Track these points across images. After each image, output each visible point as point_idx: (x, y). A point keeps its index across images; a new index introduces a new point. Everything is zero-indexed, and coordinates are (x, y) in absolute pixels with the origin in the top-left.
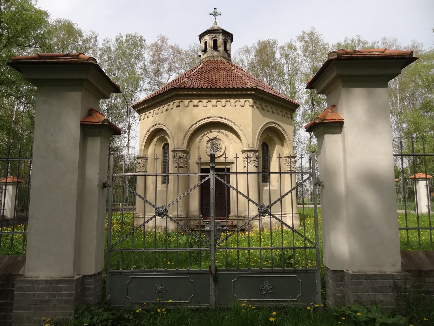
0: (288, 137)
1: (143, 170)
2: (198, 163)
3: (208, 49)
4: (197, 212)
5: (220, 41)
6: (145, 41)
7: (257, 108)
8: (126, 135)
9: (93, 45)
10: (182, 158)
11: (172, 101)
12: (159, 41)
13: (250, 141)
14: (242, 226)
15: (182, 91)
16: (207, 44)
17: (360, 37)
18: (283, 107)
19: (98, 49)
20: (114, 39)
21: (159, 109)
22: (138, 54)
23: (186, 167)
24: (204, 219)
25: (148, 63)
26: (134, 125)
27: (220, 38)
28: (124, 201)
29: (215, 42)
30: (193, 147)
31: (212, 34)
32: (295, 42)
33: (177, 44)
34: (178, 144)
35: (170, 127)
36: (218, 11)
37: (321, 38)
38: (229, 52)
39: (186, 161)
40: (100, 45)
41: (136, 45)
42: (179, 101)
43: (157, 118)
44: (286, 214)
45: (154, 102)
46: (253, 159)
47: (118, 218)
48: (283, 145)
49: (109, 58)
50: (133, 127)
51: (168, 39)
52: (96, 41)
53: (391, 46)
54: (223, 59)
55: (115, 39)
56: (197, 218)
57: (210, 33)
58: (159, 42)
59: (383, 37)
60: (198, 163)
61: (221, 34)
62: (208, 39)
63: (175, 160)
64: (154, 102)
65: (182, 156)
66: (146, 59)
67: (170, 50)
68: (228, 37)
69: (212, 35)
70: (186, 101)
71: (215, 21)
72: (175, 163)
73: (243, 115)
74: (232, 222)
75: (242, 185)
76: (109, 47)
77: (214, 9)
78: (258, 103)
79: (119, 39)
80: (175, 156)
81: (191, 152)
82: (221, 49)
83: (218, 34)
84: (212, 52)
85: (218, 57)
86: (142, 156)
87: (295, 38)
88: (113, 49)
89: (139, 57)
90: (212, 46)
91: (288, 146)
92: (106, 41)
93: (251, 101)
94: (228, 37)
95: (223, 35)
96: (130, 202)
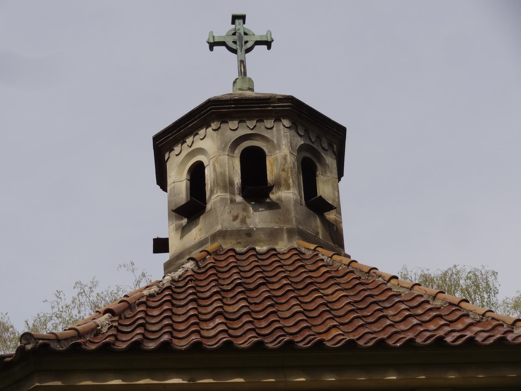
3: (215, 198)
5: (281, 149)
16: (209, 173)
29: (253, 163)
31: (233, 124)
54: (307, 247)
57: (224, 118)
62: (212, 148)
68: (322, 139)
69: (233, 130)
71: (243, 73)
77: (235, 18)
82: (289, 195)
83: (269, 123)
85: (273, 235)
90: (237, 180)
94: (322, 139)
95: (294, 126)
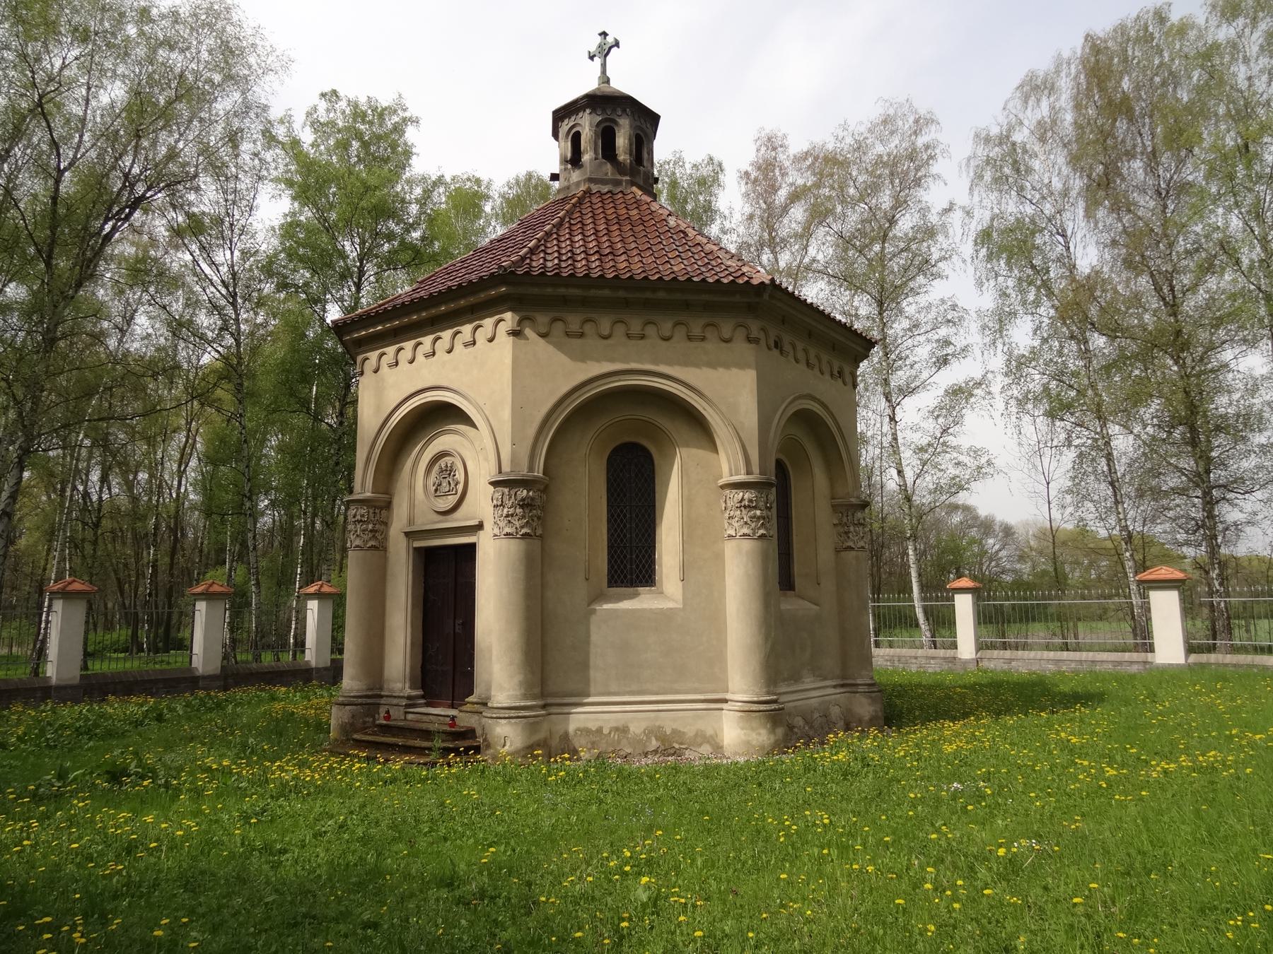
44: (726, 701)
51: (785, 136)
53: (1075, 53)
60: (407, 534)
65: (358, 517)
93: (509, 318)
94: (647, 120)
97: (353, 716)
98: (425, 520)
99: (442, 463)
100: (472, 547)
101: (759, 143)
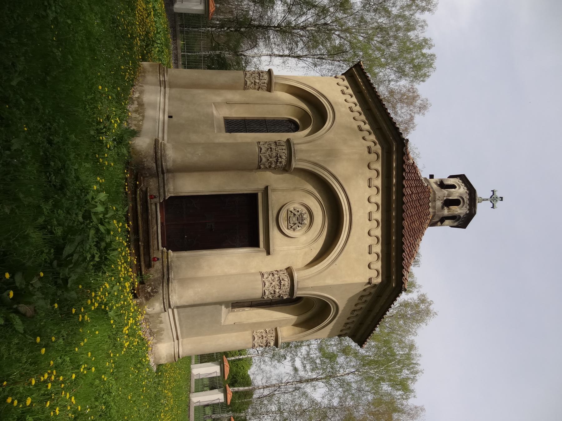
0: (310, 334)
1: (248, 83)
2: (267, 188)
3: (445, 192)
4: (174, 189)
6: (423, 81)
7: (365, 290)
8: (287, 52)
9: (417, 6)
10: (277, 160)
11: (377, 138)
12: (421, 102)
13: (310, 284)
14: (150, 283)
15: (397, 159)
17: (420, 373)
18: (361, 324)
19: (411, 12)
20: (427, 35)
21: (360, 114)
22: (405, 71)
23: (260, 168)
24: (161, 204)
25: (393, 87)
26: (305, 65)
27: (460, 206)
28: (189, 48)
29: (456, 202)
30: (297, 178)
31: (468, 197)
32: (418, 292)
33: (416, 128)
34: (302, 151)
35: (330, 135)
36: (498, 204)
37: (423, 325)
38: (439, 223)
39: (270, 167)
40: (418, 16)
41: (417, 68)
42: (380, 152)
43: (343, 109)
44: (178, 339)
45: (372, 105)
46: (277, 290)
47: (158, 36)
48: (296, 325)
49: (398, 29)
50: (301, 64)
51: (423, 114)
52: (423, 9)
55: (427, 37)
56: (162, 191)
57: (470, 194)
58: (419, 102)
59: (425, 407)
60: (267, 188)
61: (468, 212)
62: (461, 191)
63: (273, 147)
64: (372, 105)
65: (280, 160)
66: (398, 84)
67: (409, 117)
69: (466, 197)
70: (378, 166)
71: (484, 200)
72: (266, 146)
73: (355, 266)
74: (158, 259)
75: (229, 269)
76: (414, 29)
77: (502, 198)
78: (373, 291)
79: (427, 44)
80: (281, 147)
81: (286, 176)
82: (446, 212)
83: (468, 207)
84: (441, 198)
85: (434, 208)
86: (274, 80)
87: (422, 291)
88: (412, 34)
89: (401, 73)
90: (451, 198)
91: (295, 334)
92: (423, 23)
93: (379, 280)
94: (463, 222)
96: (188, 56)
97: (149, 169)
98: (275, 200)
99: (307, 222)
100: (256, 244)
101: (425, 100)
